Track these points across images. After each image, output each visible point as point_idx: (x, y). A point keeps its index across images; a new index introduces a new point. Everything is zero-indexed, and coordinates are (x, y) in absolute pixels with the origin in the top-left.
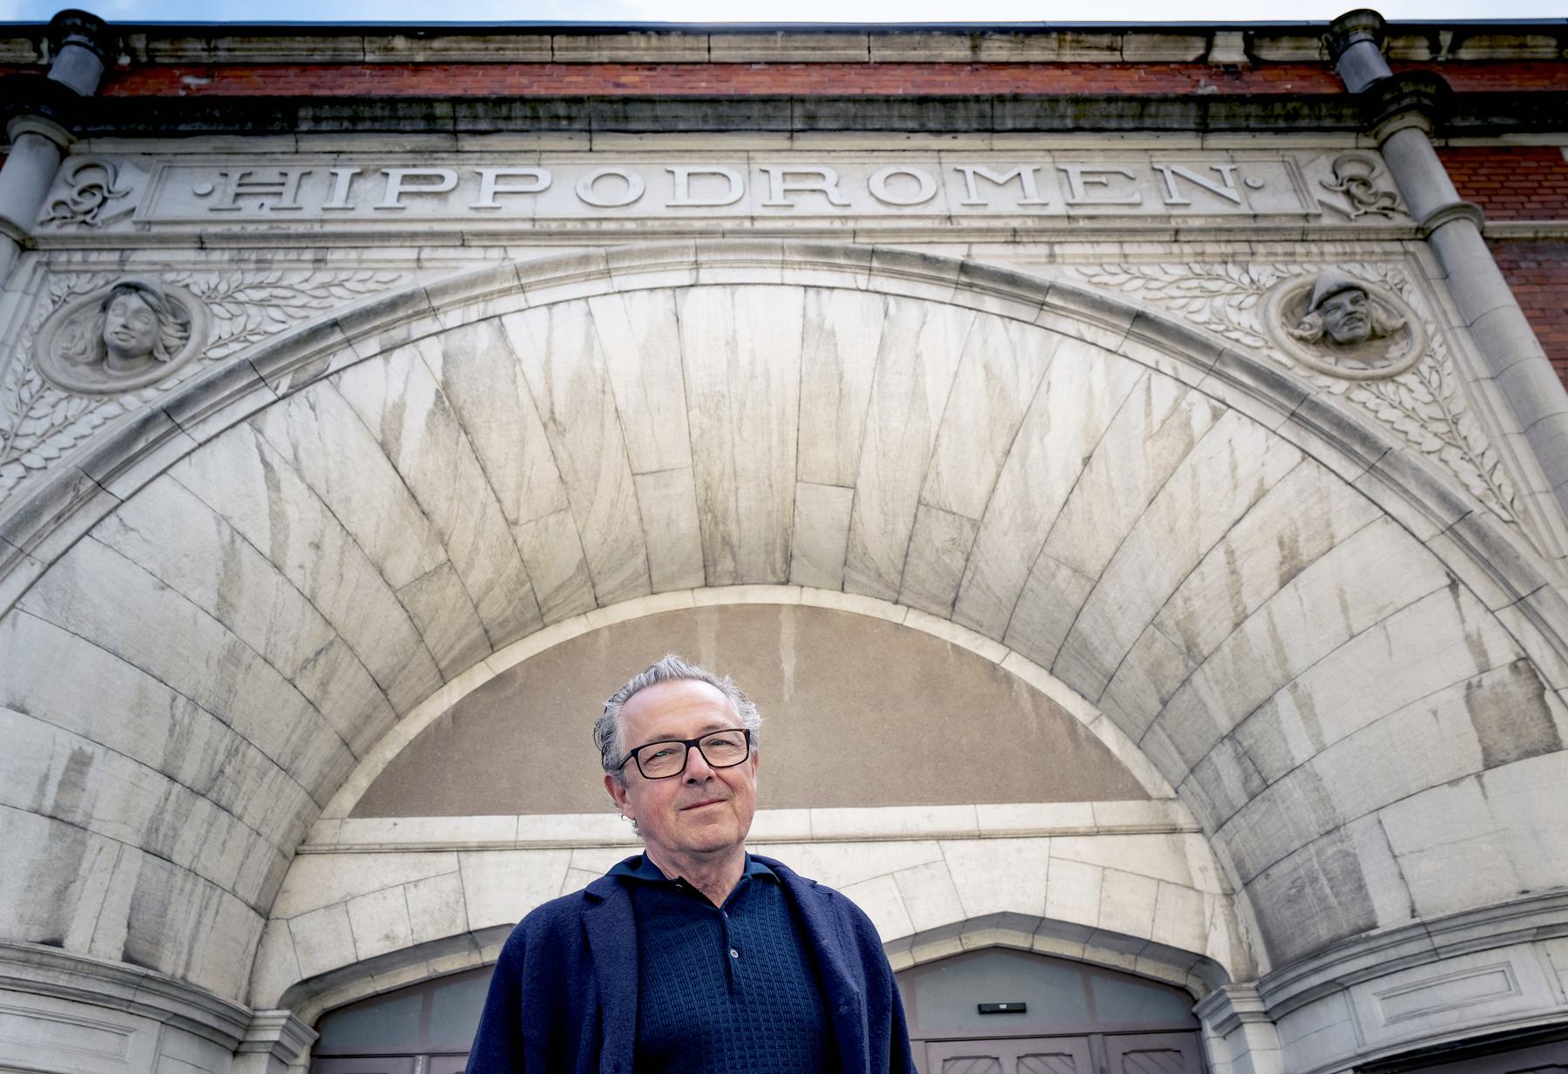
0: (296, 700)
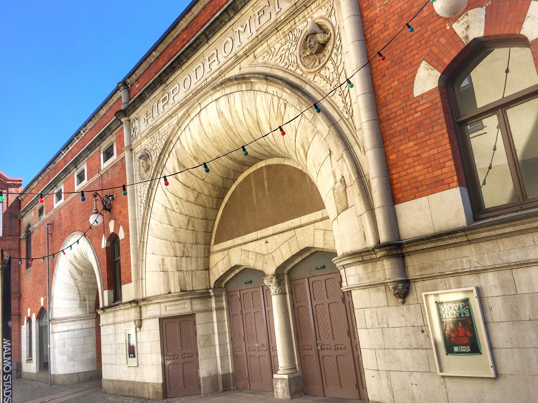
0: (190, 232)
